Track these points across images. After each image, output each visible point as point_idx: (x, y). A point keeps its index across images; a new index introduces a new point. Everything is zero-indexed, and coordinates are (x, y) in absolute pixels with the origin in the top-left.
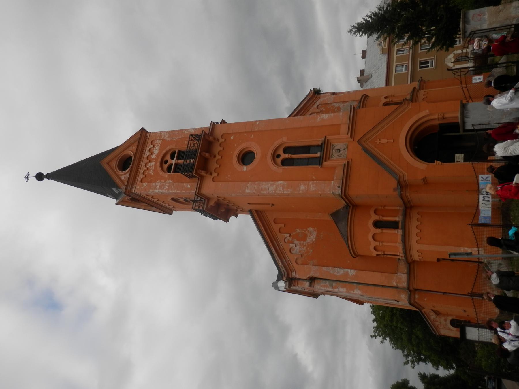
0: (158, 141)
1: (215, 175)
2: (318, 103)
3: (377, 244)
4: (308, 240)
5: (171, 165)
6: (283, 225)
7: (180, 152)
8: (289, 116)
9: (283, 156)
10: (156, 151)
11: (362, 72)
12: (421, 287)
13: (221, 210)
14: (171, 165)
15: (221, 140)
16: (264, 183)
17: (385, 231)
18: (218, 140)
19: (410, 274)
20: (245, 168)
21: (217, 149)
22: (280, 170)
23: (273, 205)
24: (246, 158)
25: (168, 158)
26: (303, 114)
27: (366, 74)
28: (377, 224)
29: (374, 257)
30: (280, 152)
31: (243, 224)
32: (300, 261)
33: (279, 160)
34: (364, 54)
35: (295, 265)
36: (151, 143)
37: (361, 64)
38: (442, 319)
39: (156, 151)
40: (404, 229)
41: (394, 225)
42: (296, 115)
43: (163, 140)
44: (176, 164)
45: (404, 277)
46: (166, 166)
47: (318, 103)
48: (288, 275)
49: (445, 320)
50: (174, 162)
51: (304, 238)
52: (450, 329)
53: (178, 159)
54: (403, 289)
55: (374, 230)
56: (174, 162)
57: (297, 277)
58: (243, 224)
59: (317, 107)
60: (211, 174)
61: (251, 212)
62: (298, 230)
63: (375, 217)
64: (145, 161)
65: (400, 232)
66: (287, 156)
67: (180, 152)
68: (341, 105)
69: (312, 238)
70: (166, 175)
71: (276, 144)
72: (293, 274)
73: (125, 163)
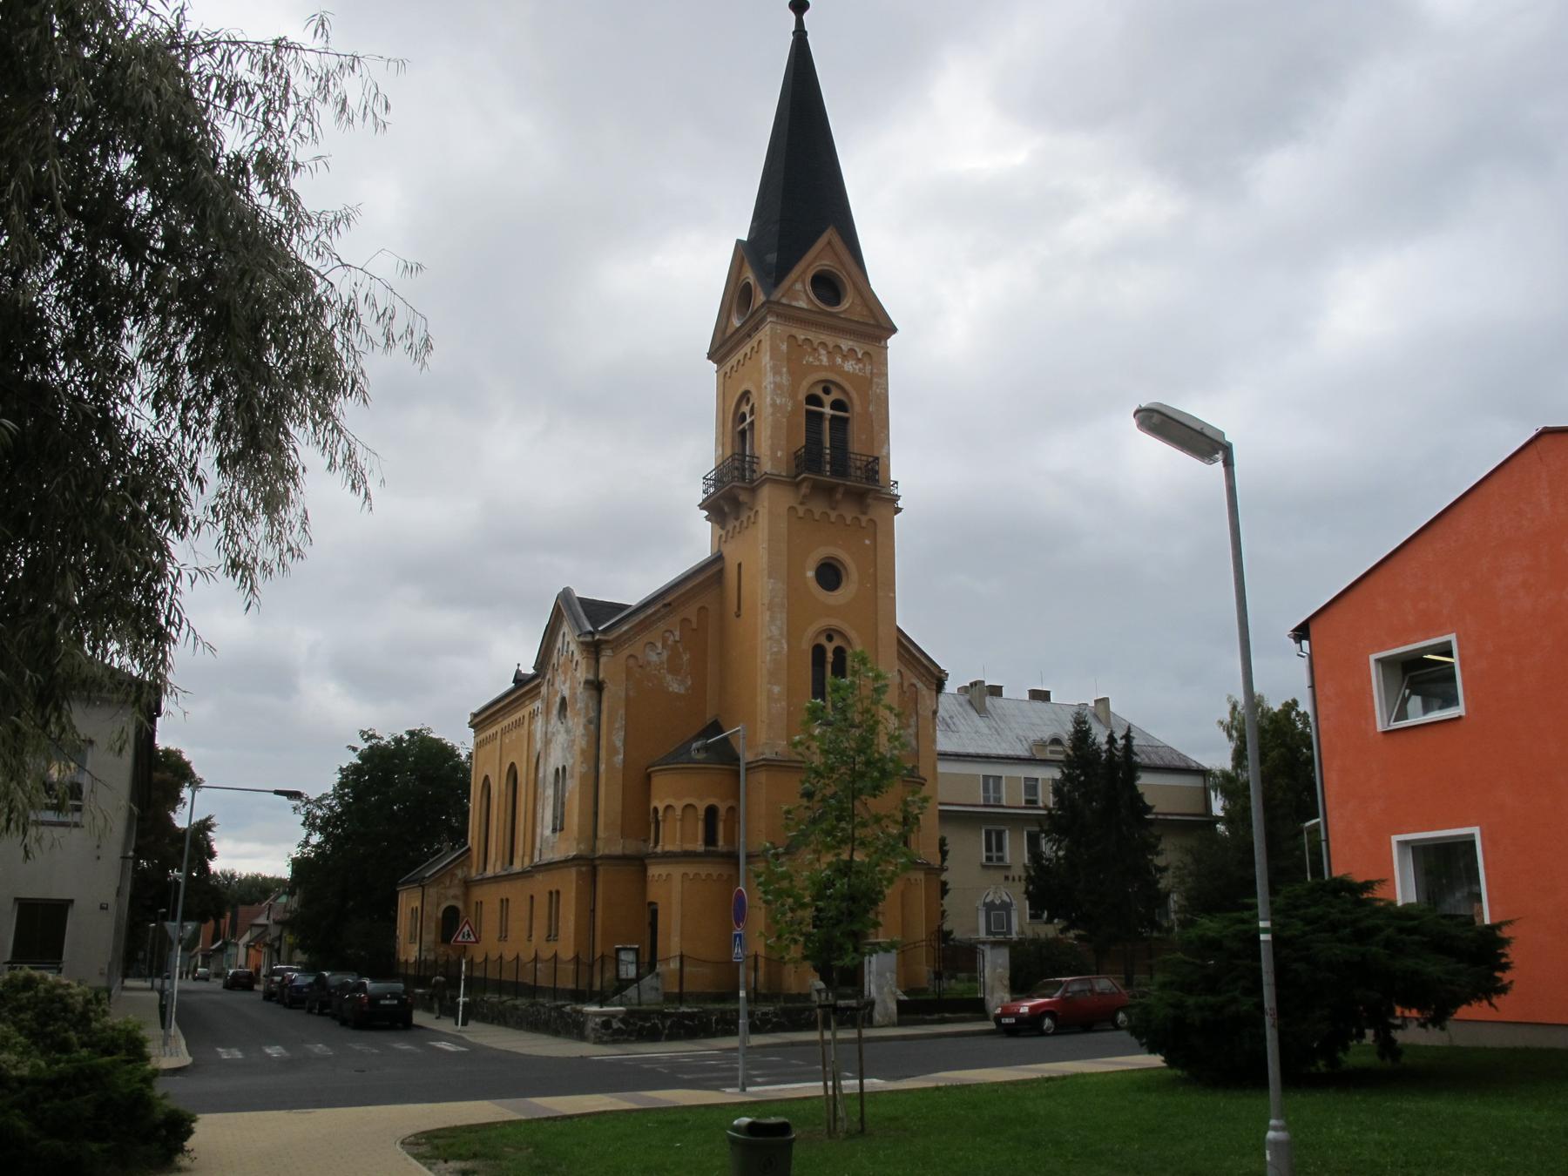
0: (868, 368)
1: (801, 511)
2: (920, 685)
3: (679, 812)
4: (669, 677)
5: (821, 404)
6: (694, 626)
7: (845, 421)
8: (899, 629)
9: (830, 648)
10: (849, 366)
11: (996, 691)
12: (600, 879)
13: (727, 500)
14: (821, 404)
15: (864, 519)
16: (784, 615)
17: (701, 825)
18: (864, 513)
19: (624, 858)
20: (810, 574)
21: (849, 512)
22: (806, 647)
23: (738, 616)
24: (830, 575)
25: (835, 395)
26: (900, 657)
27: (989, 700)
28: (711, 812)
29: (648, 801)
30: (838, 642)
31: (697, 541)
32: (632, 661)
33: (823, 641)
34: (1041, 696)
35: (626, 652)
36: (866, 353)
37: (1017, 690)
38: (456, 891)
39: (849, 366)
40: (706, 854)
41: (710, 838)
42: (899, 642)
43: (871, 381)
44: (821, 415)
45: (617, 849)
46: (819, 391)
47: (920, 685)
48: (607, 642)
49: (455, 897)
50: (827, 410)
51: (674, 669)
52: (438, 905)
53: (833, 418)
54: (594, 849)
55: (701, 807)
56: (827, 410)
57: (603, 660)
58: (697, 541)
59: (913, 685)
60: (802, 503)
61: (717, 559)
62: (686, 657)
63: (723, 809)
64: (830, 340)
65: (700, 847)
66: (830, 656)
67: (845, 421)
68: (912, 731)
69: (675, 687)
70: (802, 397)
71: (852, 634)
72: (609, 652)
73: (826, 287)
